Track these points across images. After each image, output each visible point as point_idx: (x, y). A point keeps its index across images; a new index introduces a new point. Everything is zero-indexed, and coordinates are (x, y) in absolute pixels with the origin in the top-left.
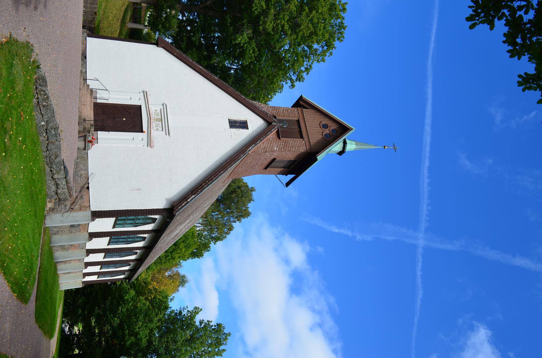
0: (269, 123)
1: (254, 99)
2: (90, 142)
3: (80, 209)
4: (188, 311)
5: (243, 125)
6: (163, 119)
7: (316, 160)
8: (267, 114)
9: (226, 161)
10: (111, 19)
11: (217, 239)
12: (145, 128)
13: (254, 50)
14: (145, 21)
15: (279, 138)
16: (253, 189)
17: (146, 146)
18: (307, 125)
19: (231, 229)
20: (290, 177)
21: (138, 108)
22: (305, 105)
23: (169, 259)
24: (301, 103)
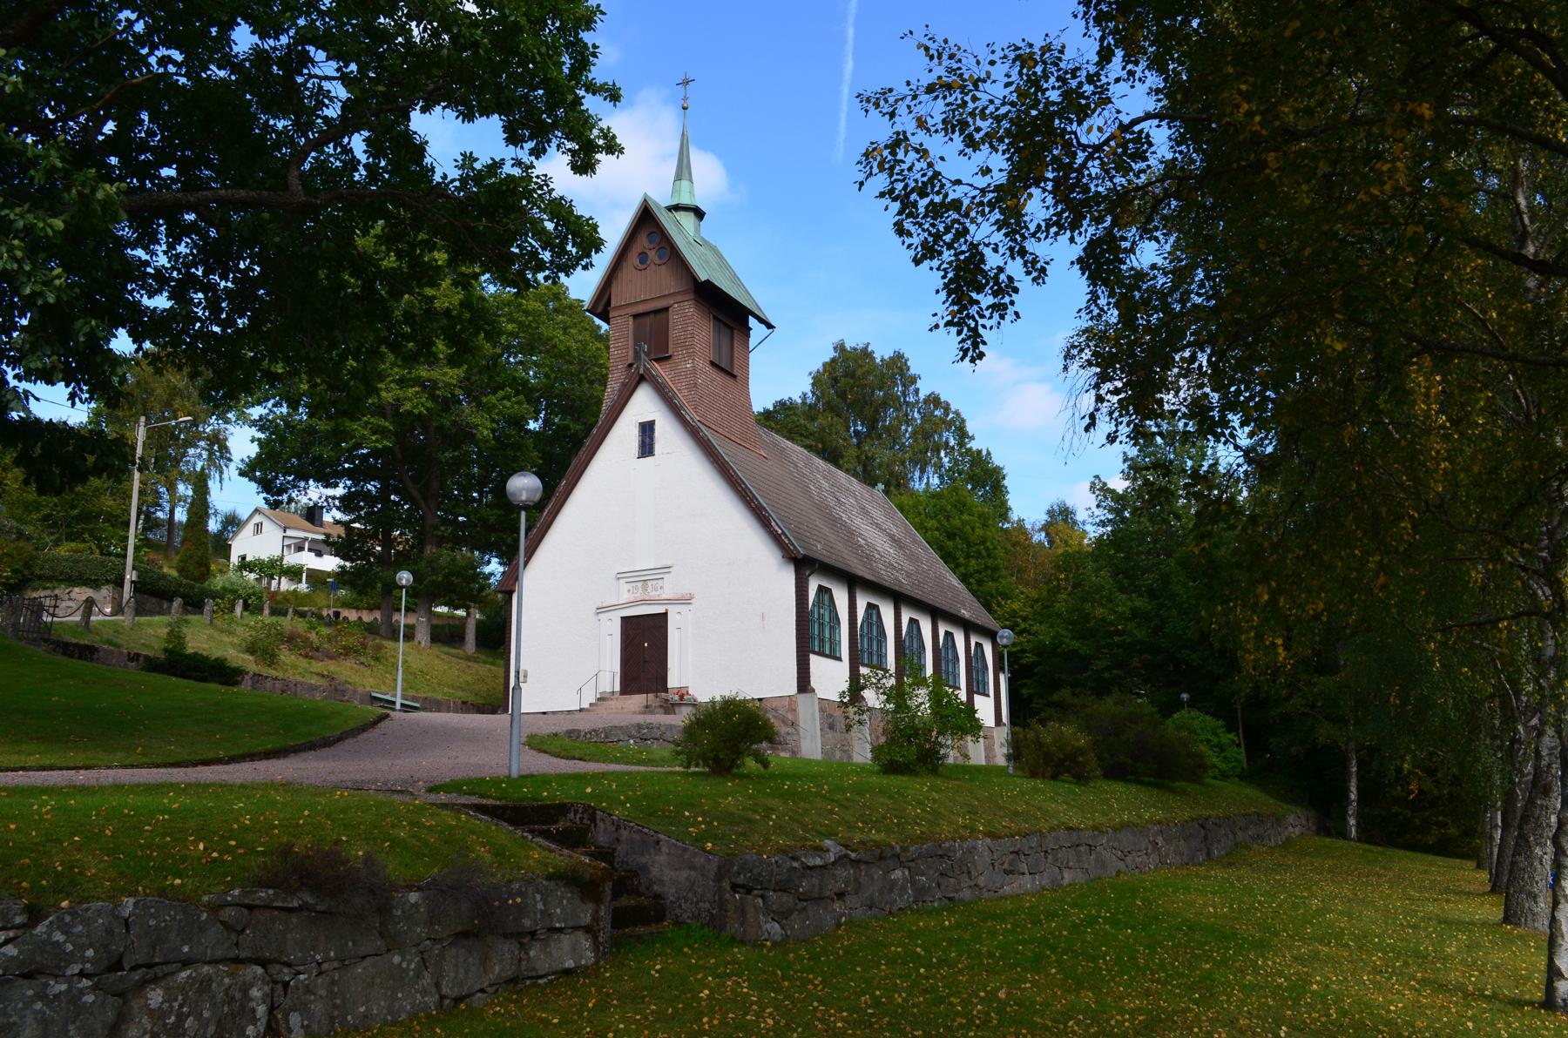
0: (642, 379)
1: (596, 414)
2: (682, 697)
3: (794, 711)
4: (1098, 506)
5: (647, 429)
6: (643, 578)
7: (708, 282)
8: (624, 385)
9: (712, 463)
10: (469, 678)
11: (962, 434)
12: (659, 610)
13: (503, 398)
14: (453, 617)
15: (670, 357)
16: (840, 348)
17: (691, 607)
18: (643, 297)
19: (934, 400)
20: (752, 322)
21: (626, 621)
22: (604, 301)
23: (987, 549)
24: (600, 309)
